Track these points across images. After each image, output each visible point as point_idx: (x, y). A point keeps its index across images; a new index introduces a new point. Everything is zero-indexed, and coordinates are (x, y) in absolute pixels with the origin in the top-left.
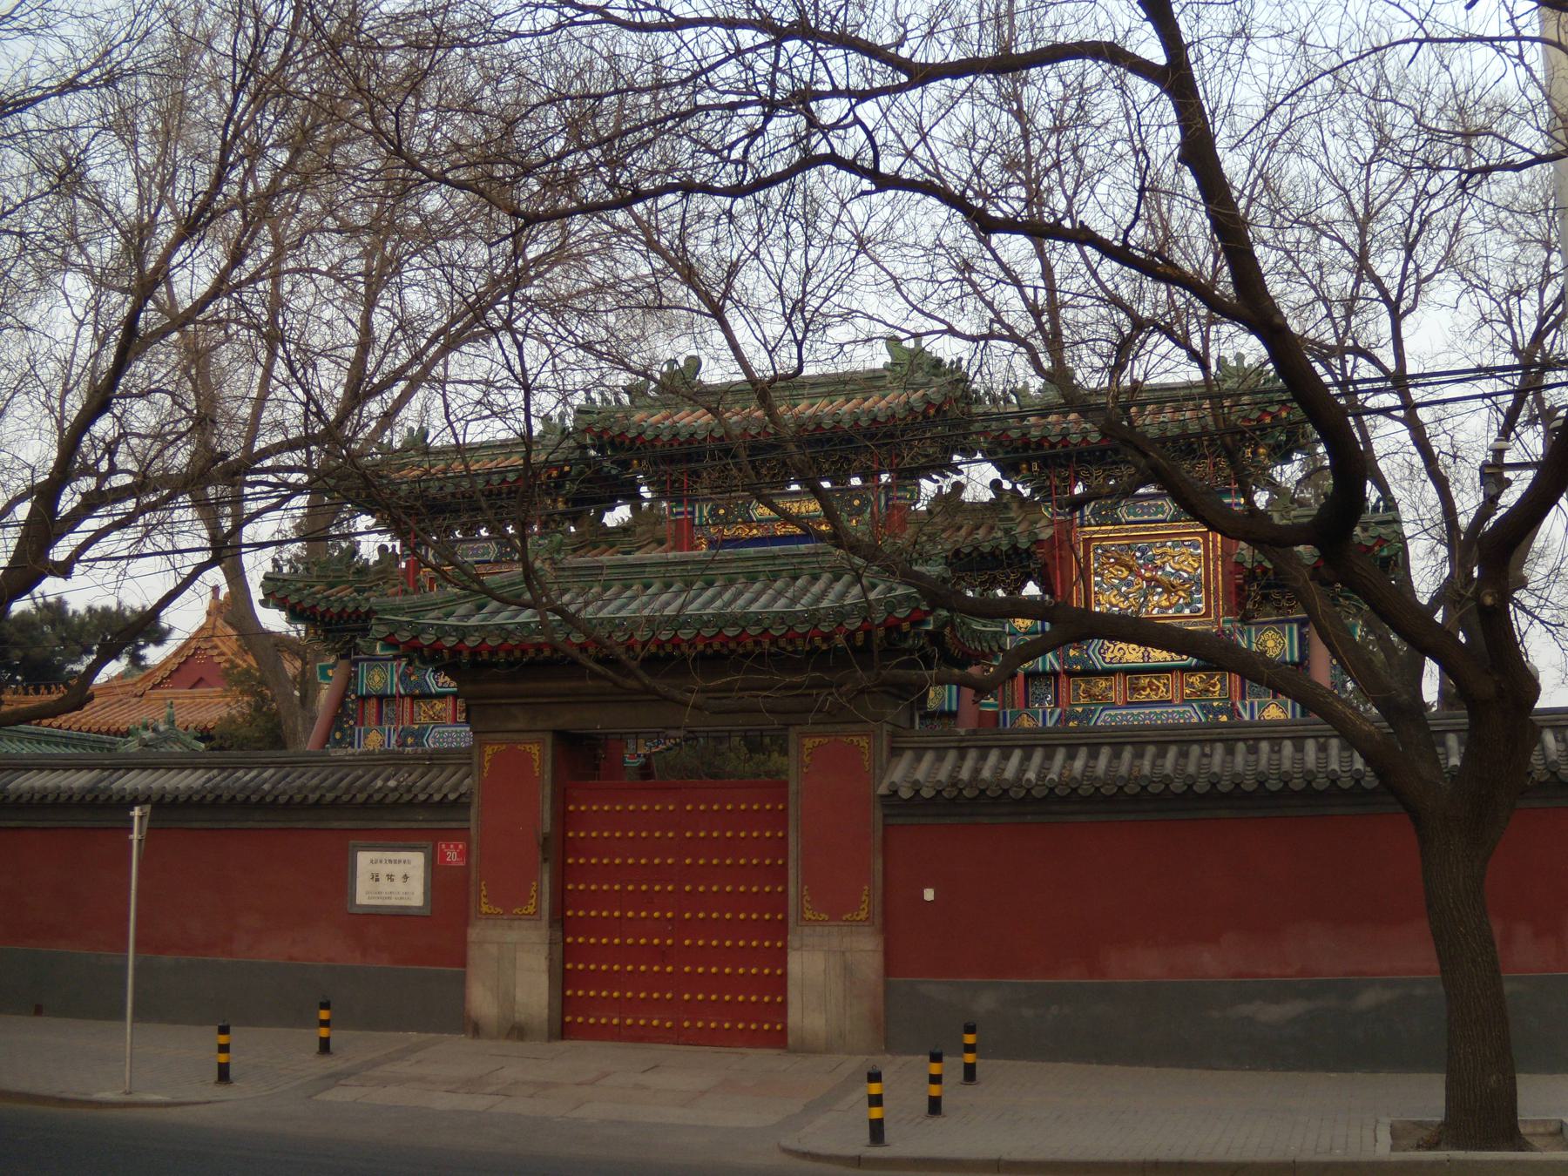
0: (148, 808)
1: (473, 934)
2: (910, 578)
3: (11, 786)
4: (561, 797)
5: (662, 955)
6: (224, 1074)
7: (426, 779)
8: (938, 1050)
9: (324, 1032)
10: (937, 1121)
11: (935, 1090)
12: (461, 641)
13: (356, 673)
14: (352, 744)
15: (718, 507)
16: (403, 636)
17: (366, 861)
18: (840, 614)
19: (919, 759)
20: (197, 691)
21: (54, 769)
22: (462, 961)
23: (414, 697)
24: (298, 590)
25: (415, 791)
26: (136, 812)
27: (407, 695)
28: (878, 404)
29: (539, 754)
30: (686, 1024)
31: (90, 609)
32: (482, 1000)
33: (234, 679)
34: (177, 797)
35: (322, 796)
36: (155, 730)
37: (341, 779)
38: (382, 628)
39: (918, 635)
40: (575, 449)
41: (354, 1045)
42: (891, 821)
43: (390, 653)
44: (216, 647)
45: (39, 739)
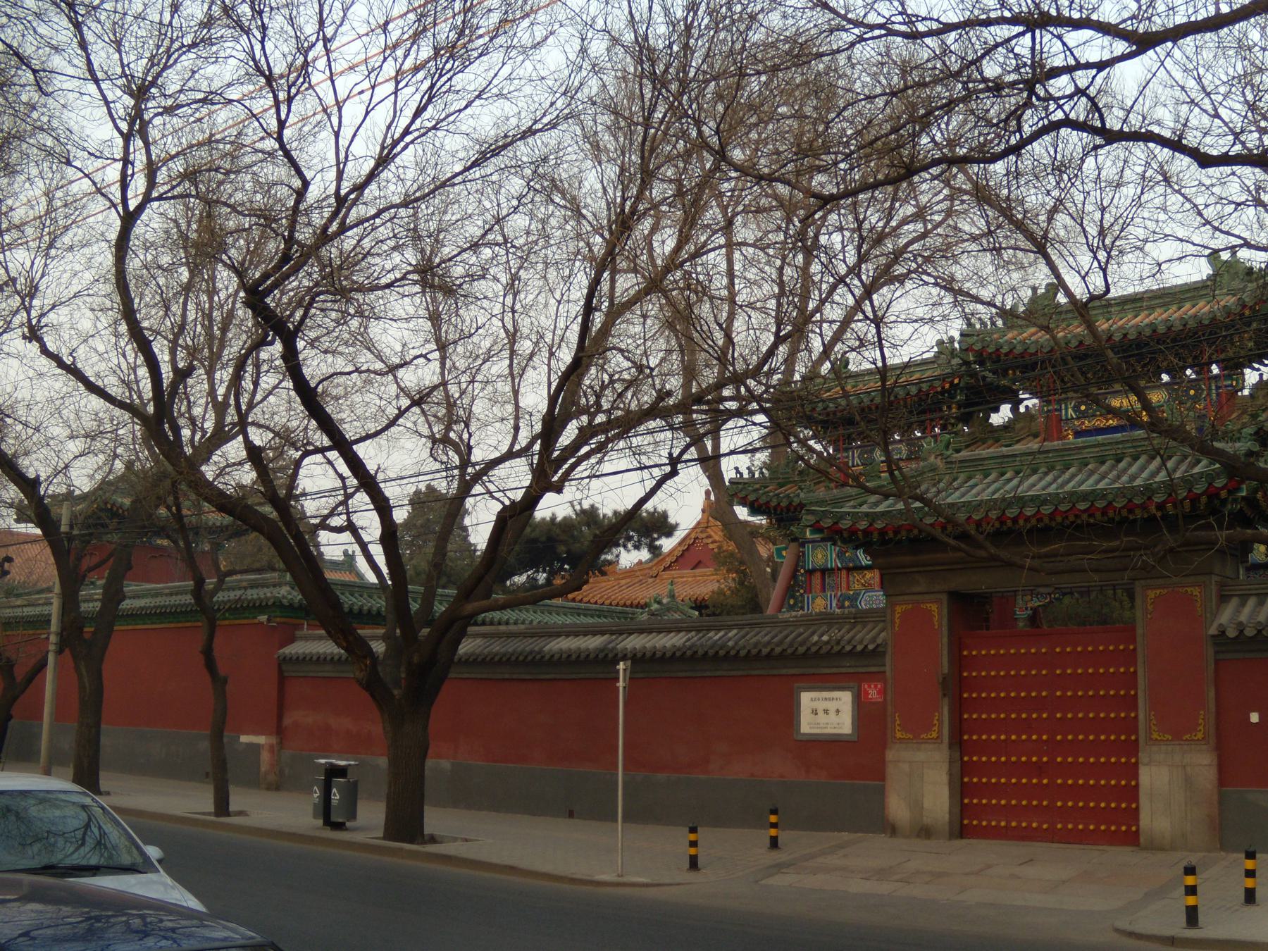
0: (629, 663)
1: (890, 755)
2: (1215, 455)
3: (547, 648)
4: (957, 645)
5: (1040, 769)
6: (694, 863)
7: (851, 634)
8: (1251, 849)
9: (773, 832)
10: (1251, 909)
11: (1250, 883)
12: (871, 525)
13: (804, 553)
14: (802, 608)
15: (1080, 404)
16: (827, 523)
17: (807, 699)
18: (1148, 490)
19: (1243, 604)
20: (697, 571)
21: (576, 634)
22: (882, 777)
23: (849, 570)
24: (757, 490)
25: (842, 643)
26: (621, 666)
27: (843, 568)
28: (1203, 308)
29: (938, 611)
30: (1059, 826)
31: (615, 513)
32: (897, 808)
33: (722, 560)
34: (654, 653)
35: (772, 650)
36: (659, 603)
37: (786, 637)
38: (809, 517)
39: (1235, 501)
40: (961, 365)
41: (796, 842)
42: (1221, 656)
43: (816, 536)
44: (709, 537)
45: (559, 610)
